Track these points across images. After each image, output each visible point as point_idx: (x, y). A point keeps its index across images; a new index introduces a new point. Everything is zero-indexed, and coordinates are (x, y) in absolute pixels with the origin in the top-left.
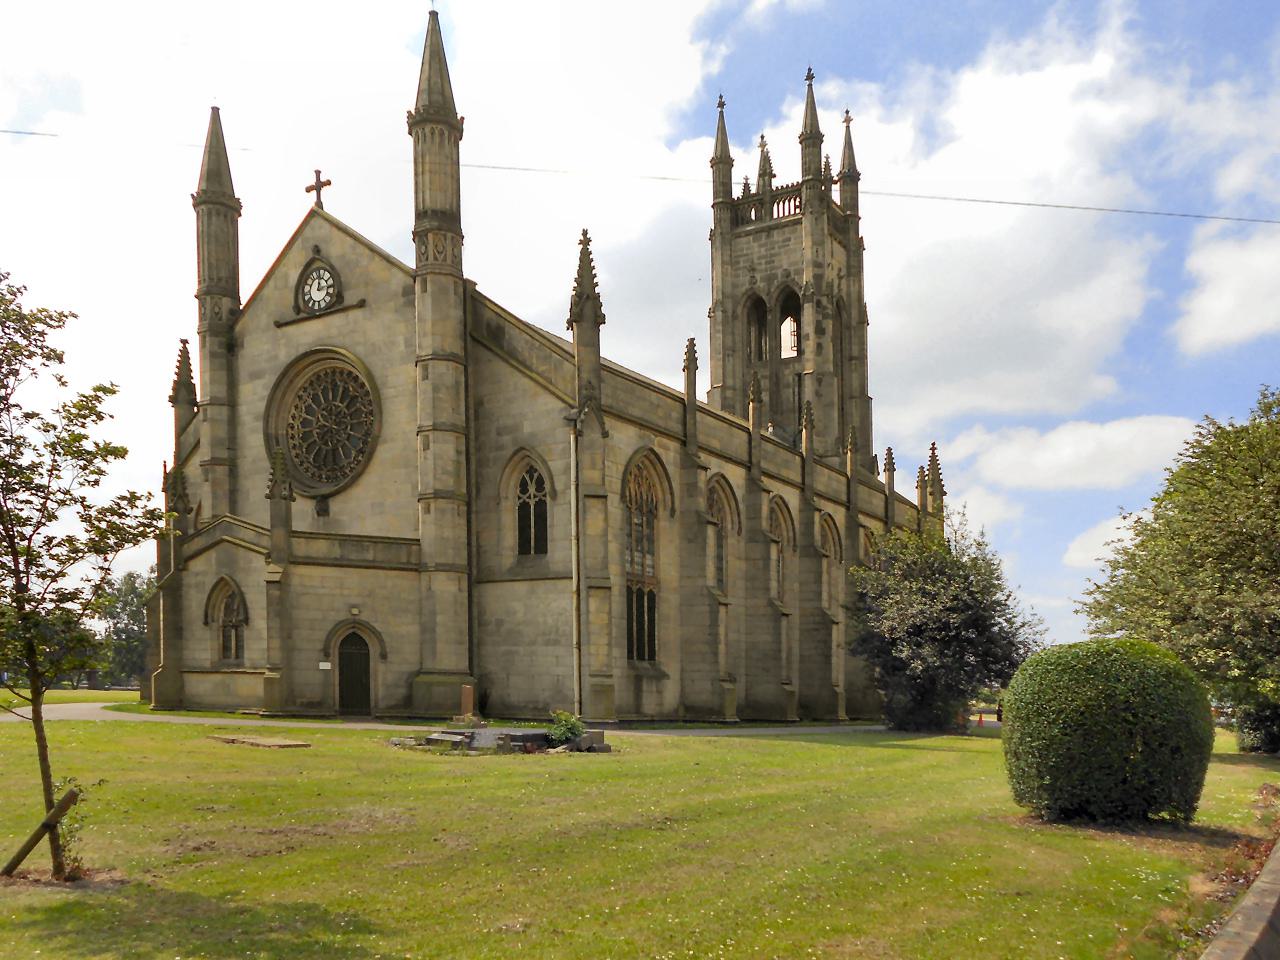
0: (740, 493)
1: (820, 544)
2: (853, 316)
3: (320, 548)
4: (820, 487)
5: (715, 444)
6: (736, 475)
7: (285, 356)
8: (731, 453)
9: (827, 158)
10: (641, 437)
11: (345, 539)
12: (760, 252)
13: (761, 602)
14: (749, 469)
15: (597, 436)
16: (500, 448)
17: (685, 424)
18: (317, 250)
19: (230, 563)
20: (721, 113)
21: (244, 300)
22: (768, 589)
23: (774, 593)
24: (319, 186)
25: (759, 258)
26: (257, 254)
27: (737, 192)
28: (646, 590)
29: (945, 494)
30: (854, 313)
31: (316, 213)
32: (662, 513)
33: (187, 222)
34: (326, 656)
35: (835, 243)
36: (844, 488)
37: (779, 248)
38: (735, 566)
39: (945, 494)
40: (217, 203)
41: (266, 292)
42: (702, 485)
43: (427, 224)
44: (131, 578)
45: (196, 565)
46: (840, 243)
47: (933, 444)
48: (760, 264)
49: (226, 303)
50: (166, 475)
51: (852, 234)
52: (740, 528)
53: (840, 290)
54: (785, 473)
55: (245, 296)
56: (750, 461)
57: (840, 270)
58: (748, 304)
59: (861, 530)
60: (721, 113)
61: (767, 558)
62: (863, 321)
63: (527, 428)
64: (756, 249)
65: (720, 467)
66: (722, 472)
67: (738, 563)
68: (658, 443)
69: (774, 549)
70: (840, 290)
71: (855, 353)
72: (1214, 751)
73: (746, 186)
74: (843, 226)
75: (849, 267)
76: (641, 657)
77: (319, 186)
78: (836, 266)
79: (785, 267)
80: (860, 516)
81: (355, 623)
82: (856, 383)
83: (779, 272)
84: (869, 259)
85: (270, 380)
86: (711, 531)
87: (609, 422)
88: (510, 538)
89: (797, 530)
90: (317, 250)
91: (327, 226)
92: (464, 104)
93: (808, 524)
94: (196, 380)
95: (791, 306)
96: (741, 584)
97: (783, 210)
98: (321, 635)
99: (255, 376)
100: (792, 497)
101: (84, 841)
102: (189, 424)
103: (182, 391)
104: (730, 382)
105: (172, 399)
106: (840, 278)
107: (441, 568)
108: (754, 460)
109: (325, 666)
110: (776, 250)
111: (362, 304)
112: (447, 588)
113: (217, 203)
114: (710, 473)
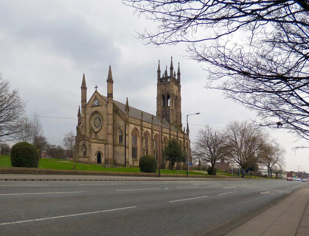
3: (95, 141)
5: (146, 126)
6: (150, 131)
7: (92, 112)
8: (149, 127)
10: (135, 126)
11: (98, 140)
14: (152, 130)
15: (128, 126)
16: (117, 127)
17: (141, 124)
18: (96, 97)
19: (84, 142)
21: (87, 102)
22: (154, 148)
24: (96, 87)
26: (88, 98)
27: (161, 77)
28: (135, 148)
30: (179, 98)
31: (96, 91)
32: (138, 137)
33: (80, 91)
34: (96, 156)
36: (169, 131)
40: (84, 88)
41: (90, 102)
42: (143, 133)
43: (109, 96)
45: (81, 142)
49: (85, 103)
50: (77, 127)
55: (87, 102)
61: (154, 143)
63: (120, 125)
68: (137, 127)
69: (155, 142)
71: (179, 105)
73: (163, 75)
74: (178, 82)
75: (178, 90)
76: (134, 158)
77: (96, 87)
81: (99, 151)
82: (179, 111)
83: (167, 91)
84: (181, 88)
85: (90, 115)
87: (130, 124)
88: (118, 140)
90: (96, 97)
91: (97, 94)
92: (114, 78)
94: (81, 113)
97: (169, 80)
98: (95, 153)
99: (88, 114)
101: (145, 5)
102: (80, 120)
103: (79, 115)
105: (78, 116)
106: (177, 92)
107: (110, 144)
109: (96, 157)
111: (101, 106)
112: (110, 147)
113: (84, 88)
114: (145, 131)
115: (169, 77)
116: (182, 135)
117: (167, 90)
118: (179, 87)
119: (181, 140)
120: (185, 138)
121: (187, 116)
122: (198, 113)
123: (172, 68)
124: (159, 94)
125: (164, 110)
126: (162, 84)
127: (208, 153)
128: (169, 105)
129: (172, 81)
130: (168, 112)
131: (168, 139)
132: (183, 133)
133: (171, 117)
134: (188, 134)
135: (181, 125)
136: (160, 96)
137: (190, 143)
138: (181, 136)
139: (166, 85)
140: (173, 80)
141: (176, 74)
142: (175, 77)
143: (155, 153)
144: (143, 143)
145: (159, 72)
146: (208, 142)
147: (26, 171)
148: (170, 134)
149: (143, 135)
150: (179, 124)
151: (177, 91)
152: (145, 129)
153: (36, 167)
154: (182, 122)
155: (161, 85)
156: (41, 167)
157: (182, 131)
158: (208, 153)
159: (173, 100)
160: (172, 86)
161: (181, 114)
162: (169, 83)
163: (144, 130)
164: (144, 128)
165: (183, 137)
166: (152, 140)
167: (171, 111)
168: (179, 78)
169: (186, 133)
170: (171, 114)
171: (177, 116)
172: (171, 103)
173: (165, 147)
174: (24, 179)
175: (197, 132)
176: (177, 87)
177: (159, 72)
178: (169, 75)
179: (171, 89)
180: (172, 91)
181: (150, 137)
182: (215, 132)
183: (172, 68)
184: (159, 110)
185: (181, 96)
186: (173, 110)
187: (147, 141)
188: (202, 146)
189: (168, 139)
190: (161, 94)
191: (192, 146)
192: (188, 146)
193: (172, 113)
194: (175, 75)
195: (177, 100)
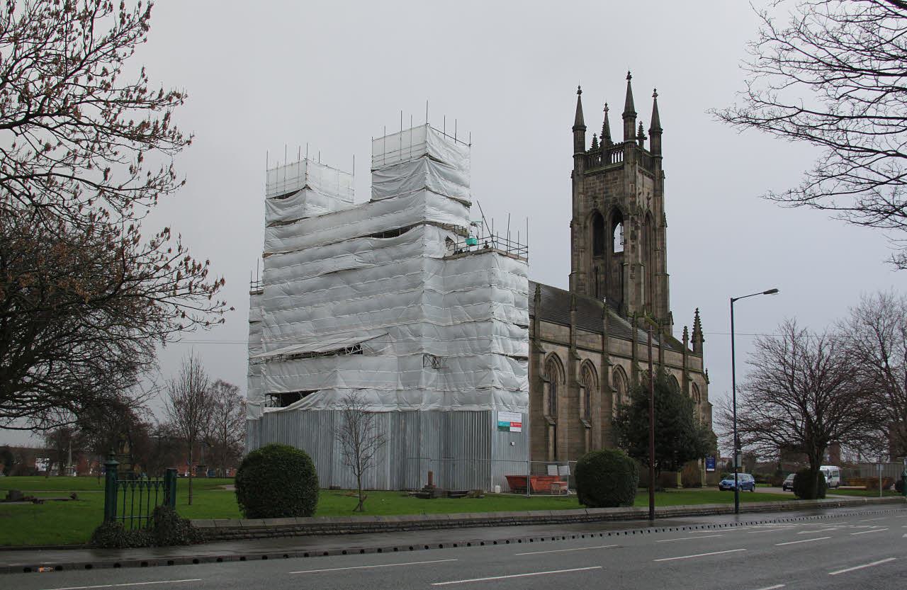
0: (564, 361)
1: (612, 384)
2: (657, 222)
4: (614, 351)
5: (551, 337)
6: (563, 352)
8: (560, 339)
9: (641, 123)
12: (600, 186)
13: (575, 421)
20: (579, 97)
22: (579, 414)
23: (582, 415)
25: (599, 190)
27: (588, 146)
29: (704, 341)
30: (658, 220)
35: (645, 177)
36: (630, 348)
37: (611, 183)
38: (563, 401)
39: (704, 341)
44: (195, 402)
46: (649, 176)
47: (697, 309)
48: (600, 194)
51: (657, 167)
52: (565, 381)
53: (648, 206)
54: (591, 346)
56: (571, 343)
57: (649, 194)
58: (593, 218)
59: (640, 373)
60: (579, 97)
61: (578, 396)
62: (663, 224)
64: (598, 184)
65: (554, 348)
66: (555, 351)
67: (564, 400)
70: (648, 206)
72: (180, 429)
73: (595, 140)
74: (652, 163)
75: (655, 190)
78: (646, 191)
79: (614, 196)
80: (640, 363)
82: (659, 265)
86: (546, 386)
89: (599, 377)
93: (605, 374)
95: (618, 217)
96: (565, 411)
97: (617, 158)
100: (596, 359)
104: (582, 269)
106: (649, 199)
108: (573, 342)
110: (609, 185)
114: (546, 354)
115: (620, 147)
116: (673, 357)
117: (614, 193)
118: (658, 179)
119: (590, 363)
120: (640, 356)
121: (733, 300)
122: (775, 291)
123: (629, 115)
124: (582, 210)
125: (601, 269)
126: (594, 174)
127: (793, 419)
128: (618, 248)
129: (631, 160)
130: (615, 275)
131: (629, 375)
132: (681, 348)
133: (630, 290)
134: (698, 351)
135: (668, 319)
136: (587, 218)
137: (708, 383)
138: (672, 362)
139: (610, 177)
140: (635, 159)
141: (646, 133)
142: (641, 143)
143: (547, 429)
144: (542, 399)
145: (579, 129)
146: (792, 383)
147: (605, 518)
148: (634, 359)
149: (542, 371)
150: (659, 316)
151: (651, 195)
152: (548, 349)
153: (309, 512)
154: (672, 307)
155: (588, 176)
156: (321, 518)
157: (677, 341)
158: (793, 419)
159: (637, 228)
160: (631, 178)
161: (665, 276)
162: (621, 167)
163: (546, 350)
164: (543, 345)
165: (680, 364)
166: (574, 385)
167: (628, 271)
168: (656, 148)
169: (690, 346)
170: (630, 280)
171: (650, 285)
172: (630, 242)
173: (620, 407)
174: (222, 564)
175: (754, 349)
176: (648, 181)
177: (579, 129)
178: (617, 137)
179: (629, 190)
180: (634, 196)
181: (567, 374)
182: (817, 343)
183: (629, 115)
184: (582, 269)
185: (667, 210)
186: (635, 267)
187: (553, 388)
188: (771, 396)
189: (629, 375)
190: (586, 207)
191: (719, 392)
192: (701, 392)
193: (632, 278)
194: (642, 138)
195: (652, 227)
